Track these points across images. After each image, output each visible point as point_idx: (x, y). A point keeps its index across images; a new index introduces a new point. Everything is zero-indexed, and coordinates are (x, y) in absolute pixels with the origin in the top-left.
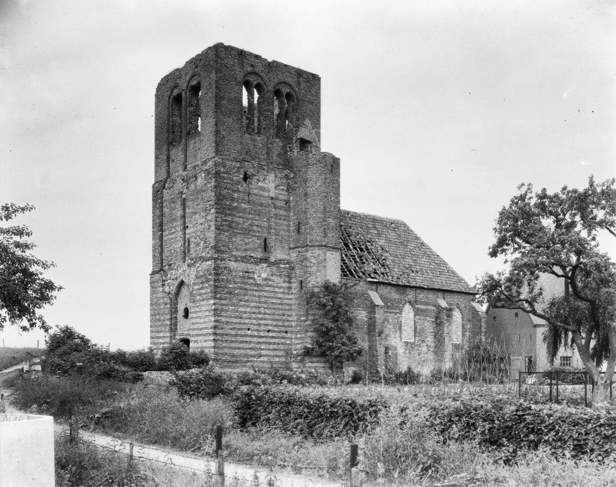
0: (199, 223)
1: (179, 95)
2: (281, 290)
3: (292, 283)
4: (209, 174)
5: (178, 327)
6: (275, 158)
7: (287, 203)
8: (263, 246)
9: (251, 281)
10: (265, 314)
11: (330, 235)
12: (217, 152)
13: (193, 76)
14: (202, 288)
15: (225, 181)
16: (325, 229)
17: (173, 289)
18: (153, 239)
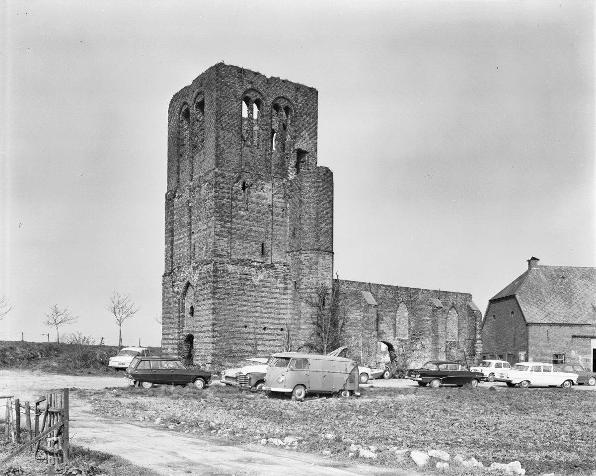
0: (202, 229)
1: (187, 110)
2: (277, 291)
3: (287, 284)
4: (210, 184)
5: (185, 324)
6: (273, 168)
7: (283, 210)
8: (261, 251)
9: (248, 282)
10: (261, 312)
11: (322, 239)
12: (217, 164)
13: (198, 94)
14: (203, 289)
15: (224, 190)
16: (317, 233)
17: (181, 289)
18: (166, 243)
